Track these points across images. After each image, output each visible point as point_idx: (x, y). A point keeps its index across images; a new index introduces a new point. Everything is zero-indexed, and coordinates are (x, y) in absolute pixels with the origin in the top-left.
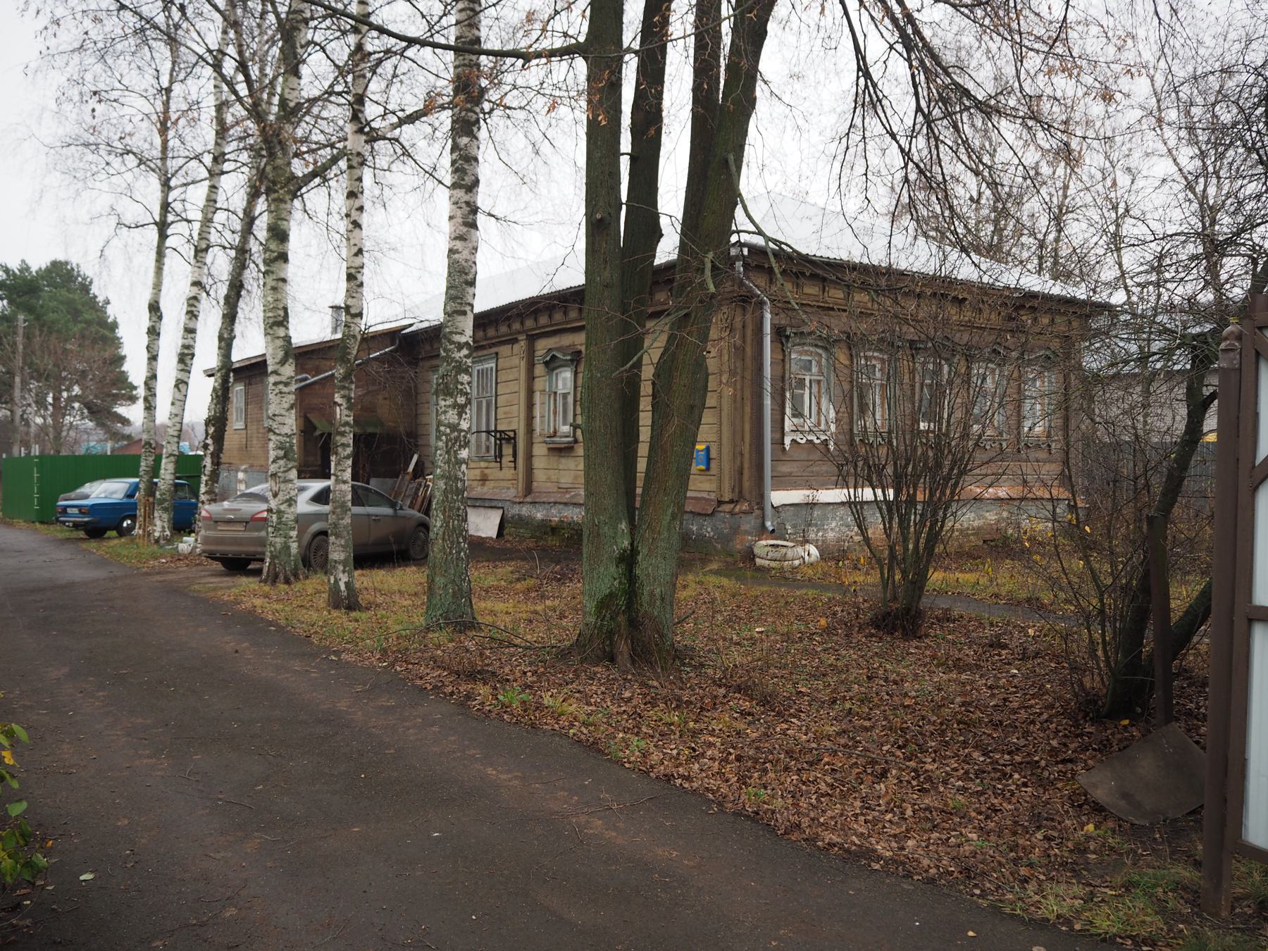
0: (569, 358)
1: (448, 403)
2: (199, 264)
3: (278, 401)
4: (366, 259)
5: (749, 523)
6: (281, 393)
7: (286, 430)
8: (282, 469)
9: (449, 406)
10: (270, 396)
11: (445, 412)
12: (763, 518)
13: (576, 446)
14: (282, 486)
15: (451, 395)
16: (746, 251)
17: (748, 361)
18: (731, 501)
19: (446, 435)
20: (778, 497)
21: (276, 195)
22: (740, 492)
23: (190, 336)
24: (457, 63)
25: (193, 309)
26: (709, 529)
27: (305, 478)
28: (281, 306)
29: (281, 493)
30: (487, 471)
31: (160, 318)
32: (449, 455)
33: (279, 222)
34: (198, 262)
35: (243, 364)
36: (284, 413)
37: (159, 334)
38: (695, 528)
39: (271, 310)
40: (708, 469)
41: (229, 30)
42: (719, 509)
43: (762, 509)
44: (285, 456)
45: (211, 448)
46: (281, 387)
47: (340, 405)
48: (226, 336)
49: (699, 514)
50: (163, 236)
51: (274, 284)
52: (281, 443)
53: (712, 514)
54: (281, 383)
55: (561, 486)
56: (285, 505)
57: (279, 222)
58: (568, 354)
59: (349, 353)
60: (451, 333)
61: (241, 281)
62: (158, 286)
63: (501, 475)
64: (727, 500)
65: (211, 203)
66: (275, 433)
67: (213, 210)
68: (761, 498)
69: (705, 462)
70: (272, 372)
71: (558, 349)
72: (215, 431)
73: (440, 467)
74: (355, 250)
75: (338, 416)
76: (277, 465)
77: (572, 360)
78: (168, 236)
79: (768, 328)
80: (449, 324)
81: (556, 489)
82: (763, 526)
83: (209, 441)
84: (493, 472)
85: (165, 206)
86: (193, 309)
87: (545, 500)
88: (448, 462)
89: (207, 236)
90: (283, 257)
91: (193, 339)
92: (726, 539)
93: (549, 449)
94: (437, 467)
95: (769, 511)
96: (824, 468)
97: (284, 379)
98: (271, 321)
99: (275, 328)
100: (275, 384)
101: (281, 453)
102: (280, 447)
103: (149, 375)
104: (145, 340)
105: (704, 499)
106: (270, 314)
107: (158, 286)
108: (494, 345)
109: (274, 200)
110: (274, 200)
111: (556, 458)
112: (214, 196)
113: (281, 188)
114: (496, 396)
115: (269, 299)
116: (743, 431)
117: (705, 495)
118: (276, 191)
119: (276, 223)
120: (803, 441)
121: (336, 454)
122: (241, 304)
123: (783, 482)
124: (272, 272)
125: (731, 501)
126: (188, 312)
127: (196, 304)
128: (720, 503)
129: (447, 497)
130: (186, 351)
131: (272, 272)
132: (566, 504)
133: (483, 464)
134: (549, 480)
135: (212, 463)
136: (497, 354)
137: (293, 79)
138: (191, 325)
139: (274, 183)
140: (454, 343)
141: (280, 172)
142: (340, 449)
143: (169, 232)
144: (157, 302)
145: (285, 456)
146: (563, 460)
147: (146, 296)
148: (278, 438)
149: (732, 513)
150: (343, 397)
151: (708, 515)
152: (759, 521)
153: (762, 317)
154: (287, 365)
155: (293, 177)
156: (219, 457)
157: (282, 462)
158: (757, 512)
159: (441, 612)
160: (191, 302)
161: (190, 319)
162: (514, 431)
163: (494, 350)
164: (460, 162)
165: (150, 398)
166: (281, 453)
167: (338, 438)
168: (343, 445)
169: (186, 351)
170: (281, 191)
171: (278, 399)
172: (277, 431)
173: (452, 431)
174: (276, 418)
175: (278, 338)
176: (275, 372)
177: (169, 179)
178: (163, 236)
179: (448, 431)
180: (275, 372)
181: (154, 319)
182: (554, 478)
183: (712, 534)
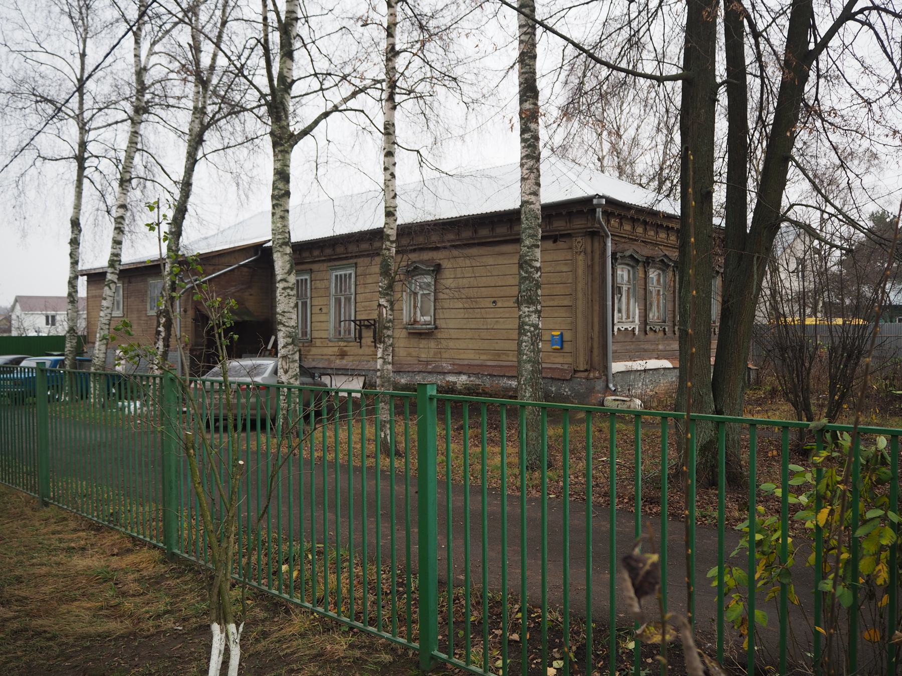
0: (432, 268)
1: (531, 309)
2: (125, 192)
3: (287, 301)
4: (398, 201)
5: (599, 385)
6: (289, 295)
7: (293, 323)
8: (291, 353)
9: (532, 312)
10: (279, 298)
11: (529, 316)
12: (607, 381)
13: (436, 331)
14: (291, 365)
15: (533, 303)
16: (604, 201)
17: (597, 275)
18: (586, 371)
19: (531, 332)
20: (617, 367)
21: (282, 148)
22: (591, 364)
23: (118, 246)
24: (523, 70)
25: (121, 226)
26: (567, 390)
27: (264, 356)
28: (287, 231)
29: (290, 370)
30: (345, 349)
31: (80, 231)
32: (534, 346)
33: (285, 168)
34: (123, 189)
35: (128, 267)
36: (291, 310)
37: (79, 244)
38: (554, 389)
39: (280, 234)
40: (562, 348)
41: (419, 43)
42: (576, 376)
43: (606, 376)
44: (293, 343)
45: (163, 334)
46: (288, 291)
47: (386, 307)
48: (174, 248)
49: (559, 379)
50: (81, 168)
51: (282, 214)
52: (290, 333)
53: (570, 380)
54: (288, 288)
55: (421, 359)
56: (293, 379)
57: (285, 168)
58: (432, 266)
59: (391, 270)
60: (532, 260)
61: (186, 207)
62: (78, 207)
63: (361, 351)
64: (582, 369)
65: (134, 145)
66: (284, 326)
67: (135, 150)
68: (606, 368)
69: (559, 342)
70: (281, 280)
71: (422, 262)
72: (166, 321)
73: (526, 355)
74: (392, 194)
75: (385, 316)
76: (287, 349)
77: (433, 271)
78: (86, 168)
79: (609, 253)
80: (529, 254)
81: (416, 362)
82: (607, 386)
83: (161, 329)
84: (353, 349)
85: (83, 145)
86: (121, 226)
87: (410, 369)
88: (533, 351)
89: (129, 169)
90: (287, 194)
91: (120, 249)
92: (582, 398)
93: (409, 333)
94: (524, 354)
95: (611, 377)
96: (633, 347)
97: (290, 285)
98: (280, 241)
99: (284, 247)
100: (284, 289)
101: (290, 340)
102: (289, 336)
103: (72, 276)
104: (68, 249)
105: (559, 369)
106: (280, 237)
107: (78, 207)
108: (356, 257)
109: (281, 151)
110: (281, 151)
111: (417, 340)
112: (135, 140)
113: (286, 143)
114: (356, 294)
115: (279, 225)
116: (592, 323)
117: (559, 366)
118: (282, 145)
119: (283, 169)
120: (623, 329)
121: (384, 342)
122: (185, 223)
123: (618, 359)
124: (281, 205)
125: (586, 371)
126: (116, 229)
127: (123, 222)
128: (576, 371)
129: (534, 376)
130: (115, 258)
131: (281, 205)
132: (429, 373)
133: (342, 344)
134: (409, 355)
135: (164, 346)
136: (356, 264)
137: (289, 61)
138: (119, 238)
139: (281, 139)
140: (533, 267)
141: (285, 130)
142: (386, 340)
143: (86, 165)
144: (78, 219)
145: (293, 343)
146: (423, 341)
147: (70, 212)
148: (287, 329)
149: (587, 379)
150: (387, 301)
151: (567, 380)
152: (605, 384)
153: (605, 244)
154: (292, 275)
155: (292, 135)
156: (168, 341)
157: (290, 347)
158: (604, 378)
159: (535, 456)
160: (119, 220)
161: (118, 233)
162: (374, 320)
163: (355, 261)
164: (532, 140)
165: (74, 294)
166: (290, 340)
167: (385, 331)
168: (388, 336)
169: (115, 258)
170: (286, 145)
171: (287, 300)
172: (286, 324)
173: (535, 329)
174: (286, 314)
175: (286, 254)
176: (284, 280)
177: (85, 124)
178: (81, 168)
179: (532, 329)
180: (284, 280)
181: (76, 232)
182: (414, 354)
183: (569, 393)
